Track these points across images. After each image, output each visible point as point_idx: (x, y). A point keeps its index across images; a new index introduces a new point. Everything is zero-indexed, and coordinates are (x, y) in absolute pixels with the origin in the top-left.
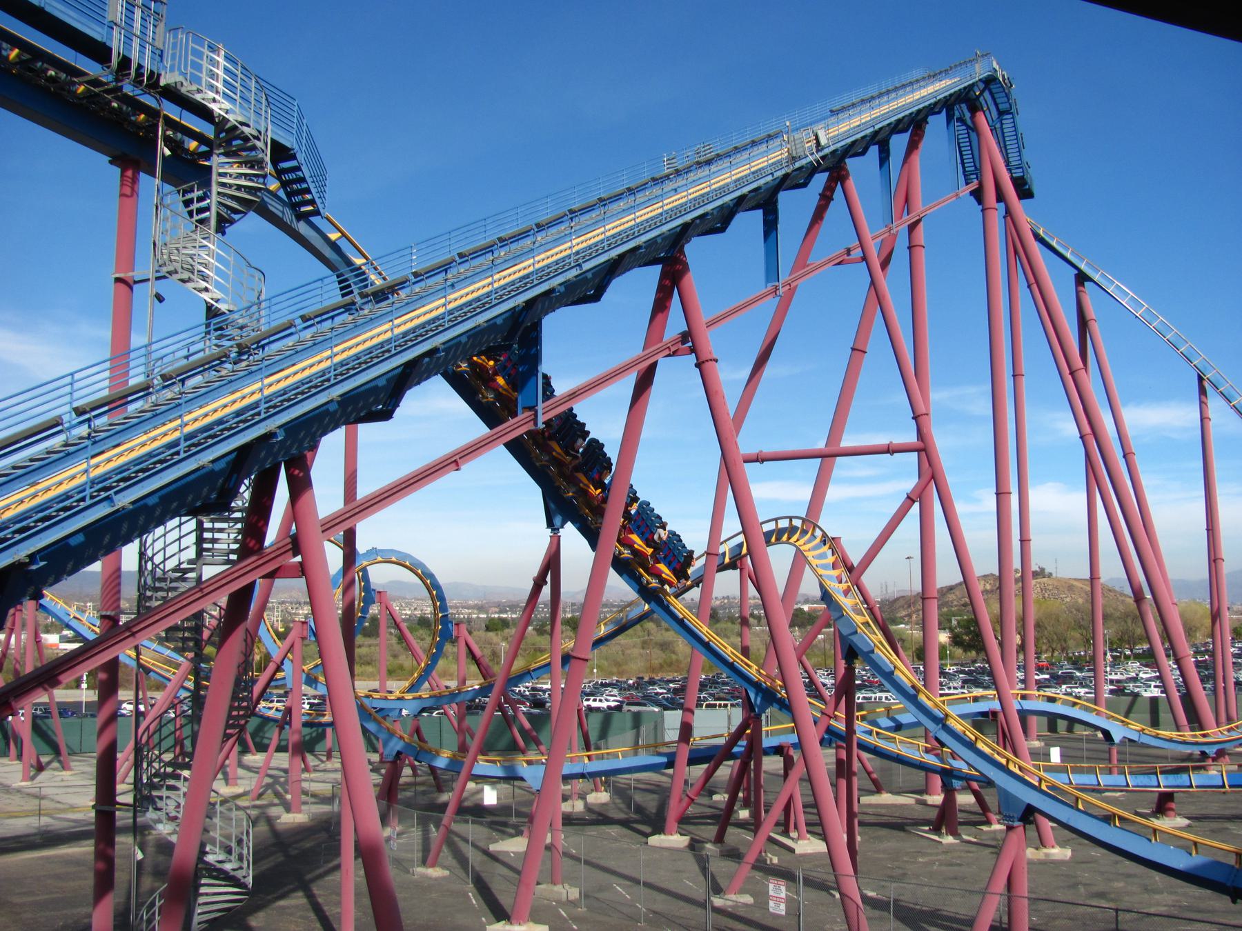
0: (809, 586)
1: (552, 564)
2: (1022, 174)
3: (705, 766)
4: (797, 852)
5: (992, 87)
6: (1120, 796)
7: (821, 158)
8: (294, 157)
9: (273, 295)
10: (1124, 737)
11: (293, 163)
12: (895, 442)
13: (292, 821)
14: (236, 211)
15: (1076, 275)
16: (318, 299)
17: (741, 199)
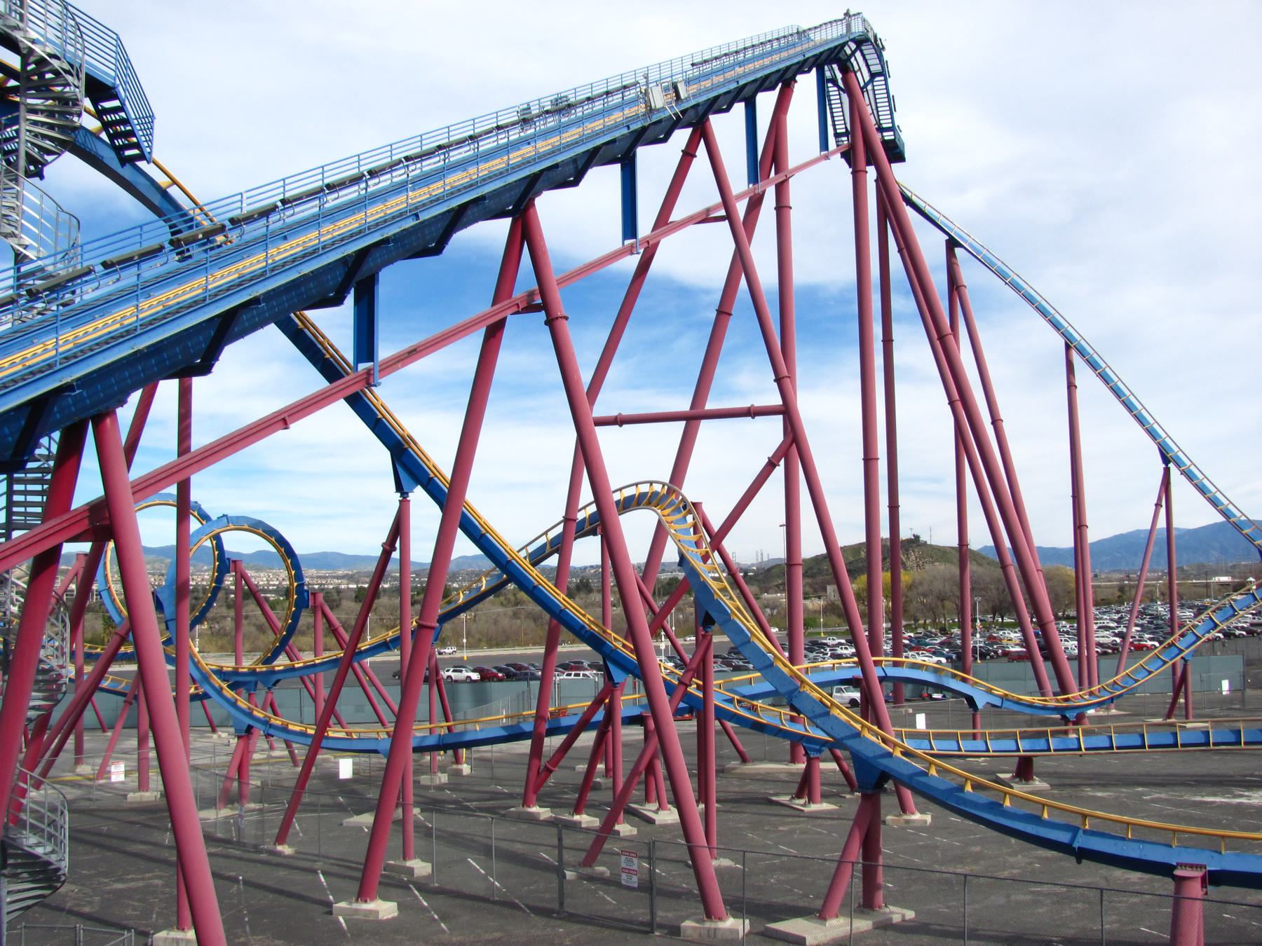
0: (670, 554)
1: (399, 529)
2: (893, 137)
3: (564, 737)
4: (657, 823)
5: (863, 48)
6: (983, 762)
7: (681, 112)
8: (116, 97)
9: (86, 241)
10: (988, 703)
11: (116, 103)
12: (756, 404)
13: (138, 800)
14: (50, 153)
15: (947, 241)
17: (596, 150)
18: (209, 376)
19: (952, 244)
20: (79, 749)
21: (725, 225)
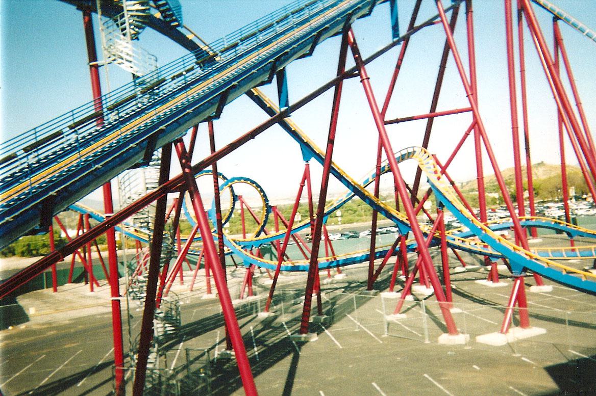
1: (306, 176)
16: (182, 66)
18: (219, 119)
19: (556, 18)
20: (182, 277)
21: (441, 24)
